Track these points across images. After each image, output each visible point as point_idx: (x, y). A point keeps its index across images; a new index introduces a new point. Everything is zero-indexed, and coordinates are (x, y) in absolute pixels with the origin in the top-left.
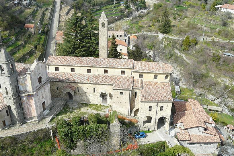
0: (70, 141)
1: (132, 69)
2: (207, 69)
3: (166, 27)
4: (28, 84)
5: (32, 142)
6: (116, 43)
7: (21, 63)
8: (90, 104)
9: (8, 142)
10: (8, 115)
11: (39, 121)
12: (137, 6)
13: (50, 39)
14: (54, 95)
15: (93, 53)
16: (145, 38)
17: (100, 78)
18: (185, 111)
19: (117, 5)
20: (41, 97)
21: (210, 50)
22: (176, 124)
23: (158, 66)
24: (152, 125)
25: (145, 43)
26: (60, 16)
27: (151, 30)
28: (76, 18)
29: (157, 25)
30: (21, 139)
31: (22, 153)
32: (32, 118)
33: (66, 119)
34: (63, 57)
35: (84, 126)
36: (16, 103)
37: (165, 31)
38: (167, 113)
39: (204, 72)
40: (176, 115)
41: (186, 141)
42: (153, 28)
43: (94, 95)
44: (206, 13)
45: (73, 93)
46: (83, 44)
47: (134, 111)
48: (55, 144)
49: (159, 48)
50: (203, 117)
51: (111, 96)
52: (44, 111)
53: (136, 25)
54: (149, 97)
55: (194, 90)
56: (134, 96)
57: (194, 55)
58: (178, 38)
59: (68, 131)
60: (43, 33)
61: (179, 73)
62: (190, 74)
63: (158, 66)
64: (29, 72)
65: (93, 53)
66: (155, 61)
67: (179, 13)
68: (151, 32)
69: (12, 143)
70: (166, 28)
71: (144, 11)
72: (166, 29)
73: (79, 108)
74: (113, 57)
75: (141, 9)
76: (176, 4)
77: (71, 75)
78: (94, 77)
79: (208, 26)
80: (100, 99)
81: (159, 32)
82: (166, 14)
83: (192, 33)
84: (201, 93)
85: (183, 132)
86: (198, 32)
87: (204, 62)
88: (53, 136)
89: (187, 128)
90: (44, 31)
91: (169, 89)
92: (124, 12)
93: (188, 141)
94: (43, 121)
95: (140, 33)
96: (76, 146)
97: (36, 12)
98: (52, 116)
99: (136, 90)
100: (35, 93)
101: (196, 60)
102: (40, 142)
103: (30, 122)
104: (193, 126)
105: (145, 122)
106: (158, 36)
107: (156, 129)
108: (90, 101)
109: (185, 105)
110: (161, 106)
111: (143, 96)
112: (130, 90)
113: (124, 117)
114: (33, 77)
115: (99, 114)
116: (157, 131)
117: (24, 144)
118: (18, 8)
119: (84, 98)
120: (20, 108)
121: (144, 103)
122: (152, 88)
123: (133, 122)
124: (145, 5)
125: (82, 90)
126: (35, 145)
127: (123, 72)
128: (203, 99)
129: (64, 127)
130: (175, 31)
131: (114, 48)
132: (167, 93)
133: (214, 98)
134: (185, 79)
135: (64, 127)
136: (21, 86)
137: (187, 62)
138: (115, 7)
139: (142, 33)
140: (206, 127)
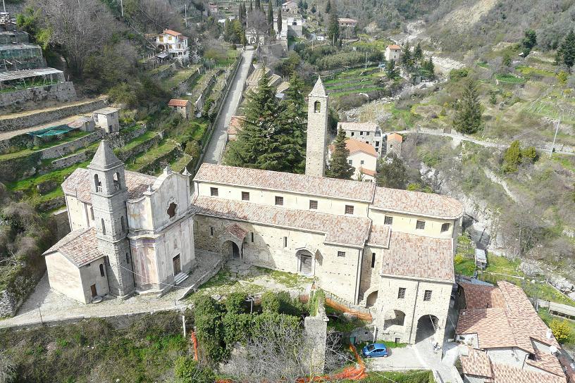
0: (217, 344)
1: (369, 203)
2: (557, 217)
3: (470, 119)
4: (145, 216)
5: (141, 335)
6: (345, 146)
7: (149, 174)
8: (274, 271)
9: (96, 328)
10: (102, 274)
11: (163, 294)
12: (414, 74)
13: (217, 132)
14: (201, 245)
15: (293, 163)
16: (419, 141)
17: (301, 218)
18: (487, 307)
19: (370, 69)
20: (172, 245)
21: (568, 175)
22: (463, 336)
23: (427, 203)
24: (404, 332)
25: (420, 151)
26: (245, 87)
27: (436, 124)
28: (266, 91)
29: (451, 113)
30: (121, 326)
31: (120, 356)
32: (149, 286)
33: (216, 297)
34: (229, 167)
35: (250, 316)
36: (119, 253)
37: (468, 129)
38: (440, 306)
39: (550, 224)
40: (464, 313)
41: (482, 377)
42: (440, 121)
43: (285, 251)
44: (567, 92)
45: (239, 245)
46: (275, 144)
47: (366, 294)
48: (189, 346)
49: (451, 163)
50: (528, 327)
51: (319, 257)
52: (176, 274)
53: (405, 113)
54: (401, 269)
55: (520, 263)
56: (368, 263)
57: (529, 185)
58: (494, 145)
59: (214, 321)
60: (205, 117)
61: (490, 221)
62: (516, 226)
63: (427, 203)
64: (148, 193)
65: (293, 163)
66: (438, 191)
67: (504, 90)
68: (435, 128)
69: (102, 332)
70: (470, 123)
71: (430, 84)
72: (470, 123)
73: (251, 275)
74: (337, 175)
75: (422, 79)
76: (499, 71)
77: (241, 206)
78: (289, 215)
79: (568, 120)
80: (296, 261)
81: (453, 131)
82: (472, 91)
83: (528, 136)
84: (536, 271)
85: (476, 355)
86: (542, 133)
87: (551, 201)
88: (186, 328)
89: (486, 347)
90: (207, 114)
91: (449, 255)
92: (383, 86)
93: (487, 378)
94: (172, 295)
95: (413, 131)
96: (229, 356)
97: (199, 77)
98: (191, 287)
99: (373, 251)
100: (158, 235)
101: (531, 195)
102: (158, 339)
103: (146, 295)
104: (502, 346)
105: (388, 323)
106: (451, 139)
107: (413, 340)
108: (276, 263)
109: (490, 294)
110: (400, 289)
111: (388, 264)
112: (360, 249)
113: (343, 305)
114: (157, 203)
115: (288, 294)
116: (414, 346)
117: (126, 337)
118: (163, 68)
119: (263, 256)
120: (128, 263)
121: (387, 279)
122: (409, 249)
123: (362, 319)
124: (432, 71)
125: (262, 239)
126: (147, 342)
127: (349, 209)
128: (540, 286)
129: (208, 312)
130: (490, 129)
131: (340, 156)
132: (443, 262)
133: (570, 286)
134: (503, 237)
135: (208, 312)
136: (132, 219)
137: (510, 199)
138: (365, 74)
139: (415, 131)
140: (532, 351)
